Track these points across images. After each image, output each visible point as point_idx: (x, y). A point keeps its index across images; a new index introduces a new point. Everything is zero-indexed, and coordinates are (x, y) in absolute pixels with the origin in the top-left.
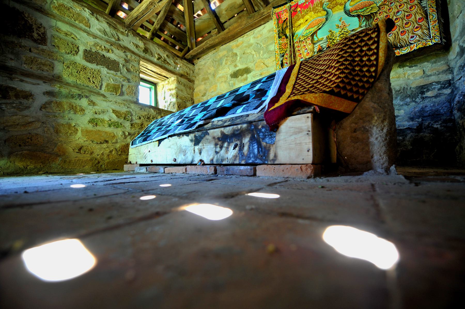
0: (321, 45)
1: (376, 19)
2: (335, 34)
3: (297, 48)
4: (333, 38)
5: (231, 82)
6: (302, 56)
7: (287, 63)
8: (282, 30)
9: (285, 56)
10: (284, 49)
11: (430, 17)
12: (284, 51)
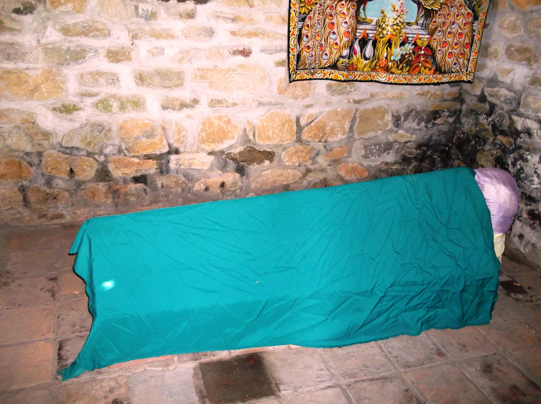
0: (367, 32)
1: (434, 22)
2: (387, 20)
3: (328, 8)
4: (384, 26)
6: (335, 30)
7: (307, 36)
9: (307, 20)
10: (306, 6)
11: (474, 46)
12: (307, 9)
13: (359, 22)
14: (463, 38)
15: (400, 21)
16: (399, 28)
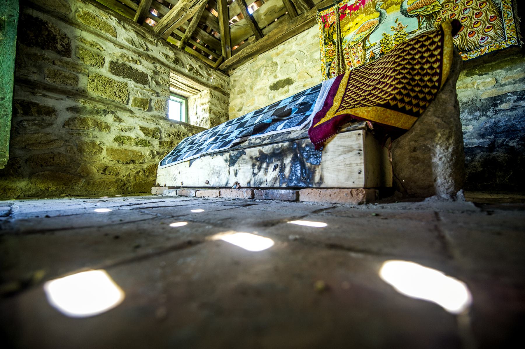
1: (439, 19)
2: (390, 38)
5: (270, 95)
6: (352, 65)
7: (334, 73)
8: (329, 35)
9: (332, 64)
13: (366, 50)
14: (484, 15)
15: (400, 34)
16: (401, 38)
